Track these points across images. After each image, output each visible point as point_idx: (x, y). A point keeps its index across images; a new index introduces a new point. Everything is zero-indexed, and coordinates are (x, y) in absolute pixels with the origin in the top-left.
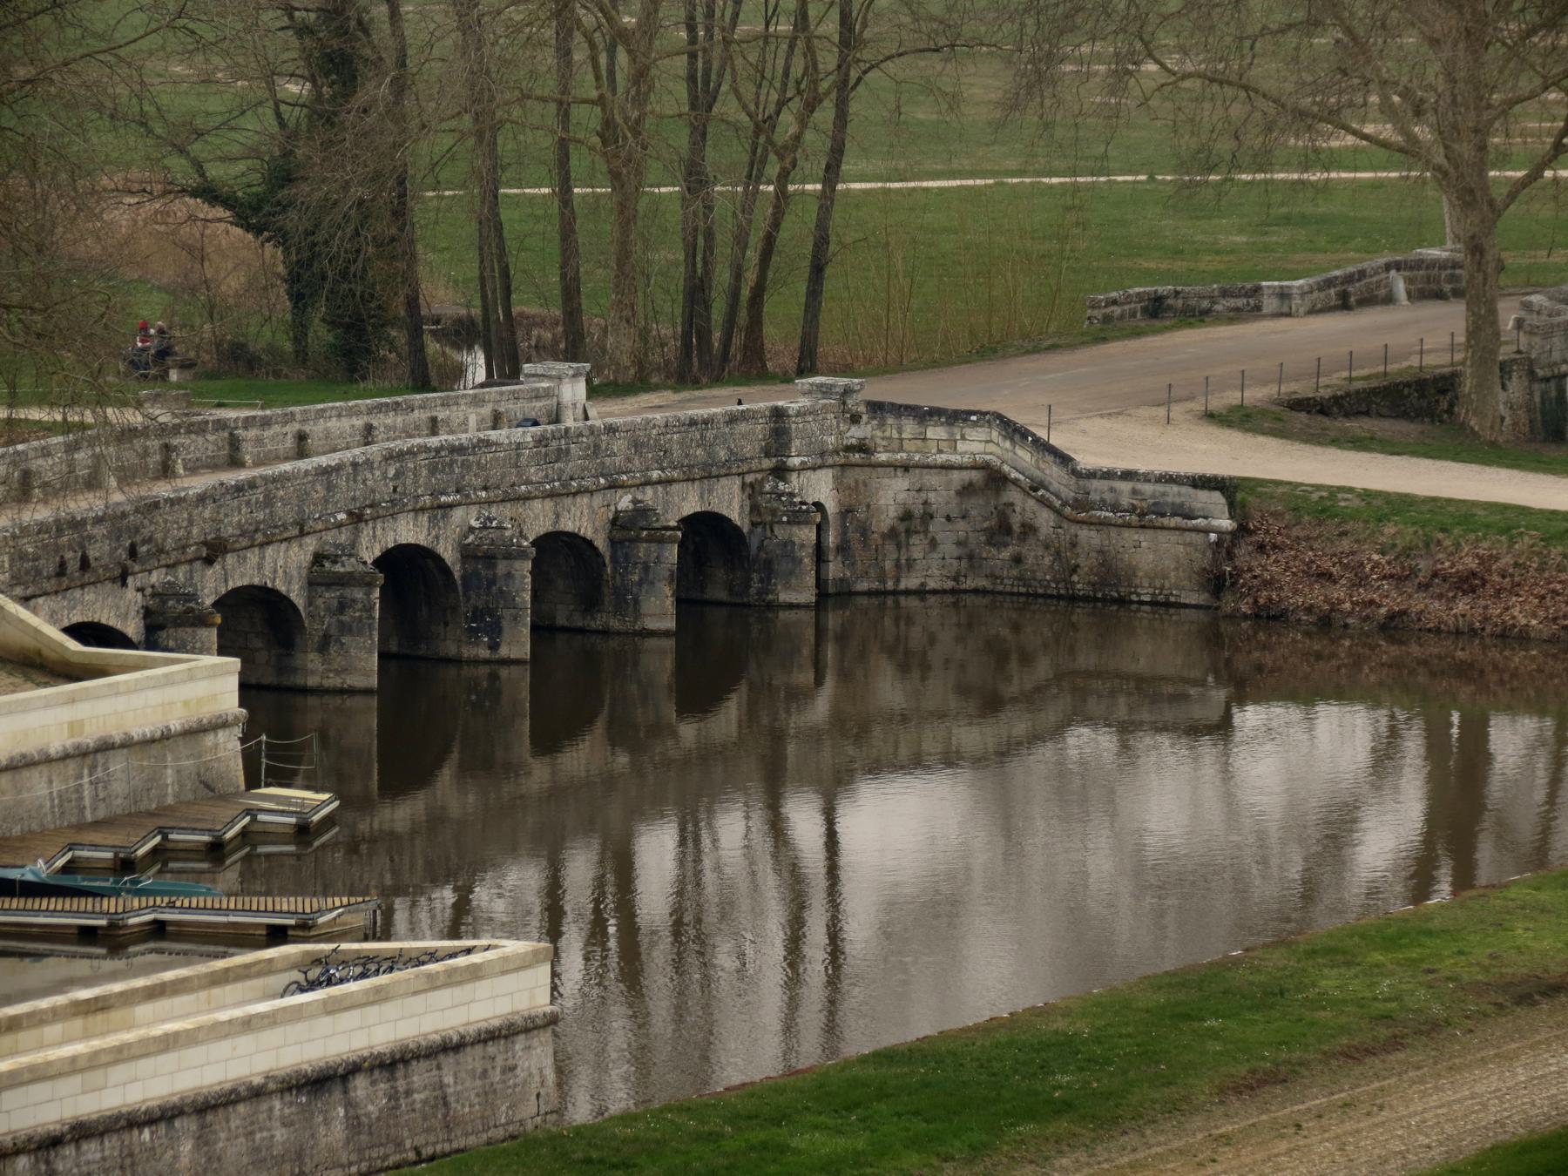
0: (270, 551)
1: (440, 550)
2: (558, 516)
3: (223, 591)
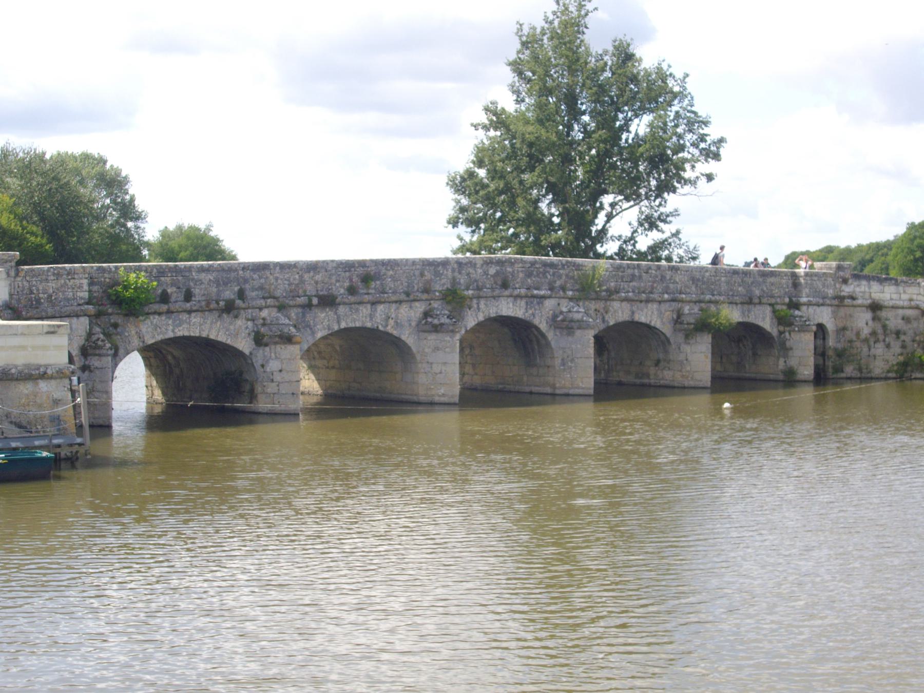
0: (380, 308)
1: (536, 321)
2: (633, 313)
3: (336, 328)
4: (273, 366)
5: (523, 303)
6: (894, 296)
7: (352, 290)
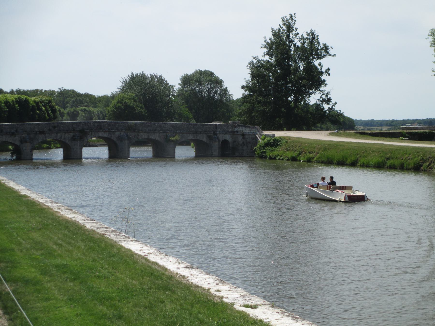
4: (24, 148)
5: (108, 133)
6: (249, 131)
7: (50, 130)
